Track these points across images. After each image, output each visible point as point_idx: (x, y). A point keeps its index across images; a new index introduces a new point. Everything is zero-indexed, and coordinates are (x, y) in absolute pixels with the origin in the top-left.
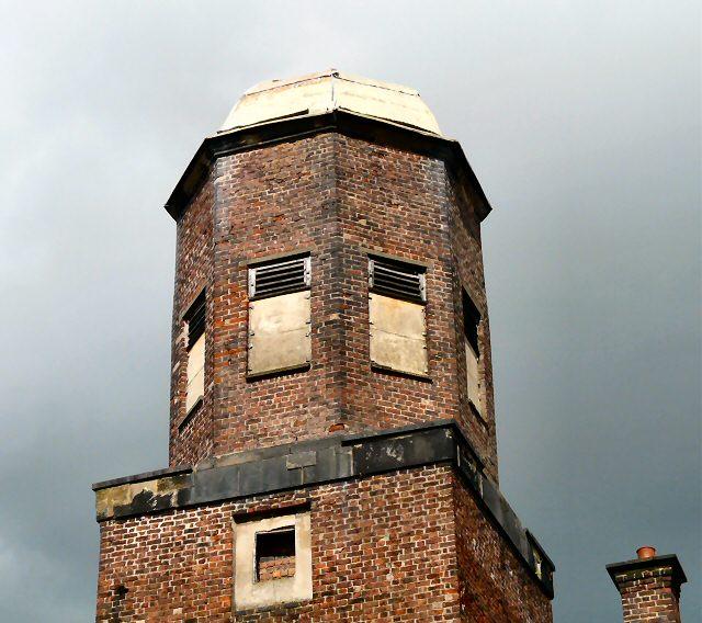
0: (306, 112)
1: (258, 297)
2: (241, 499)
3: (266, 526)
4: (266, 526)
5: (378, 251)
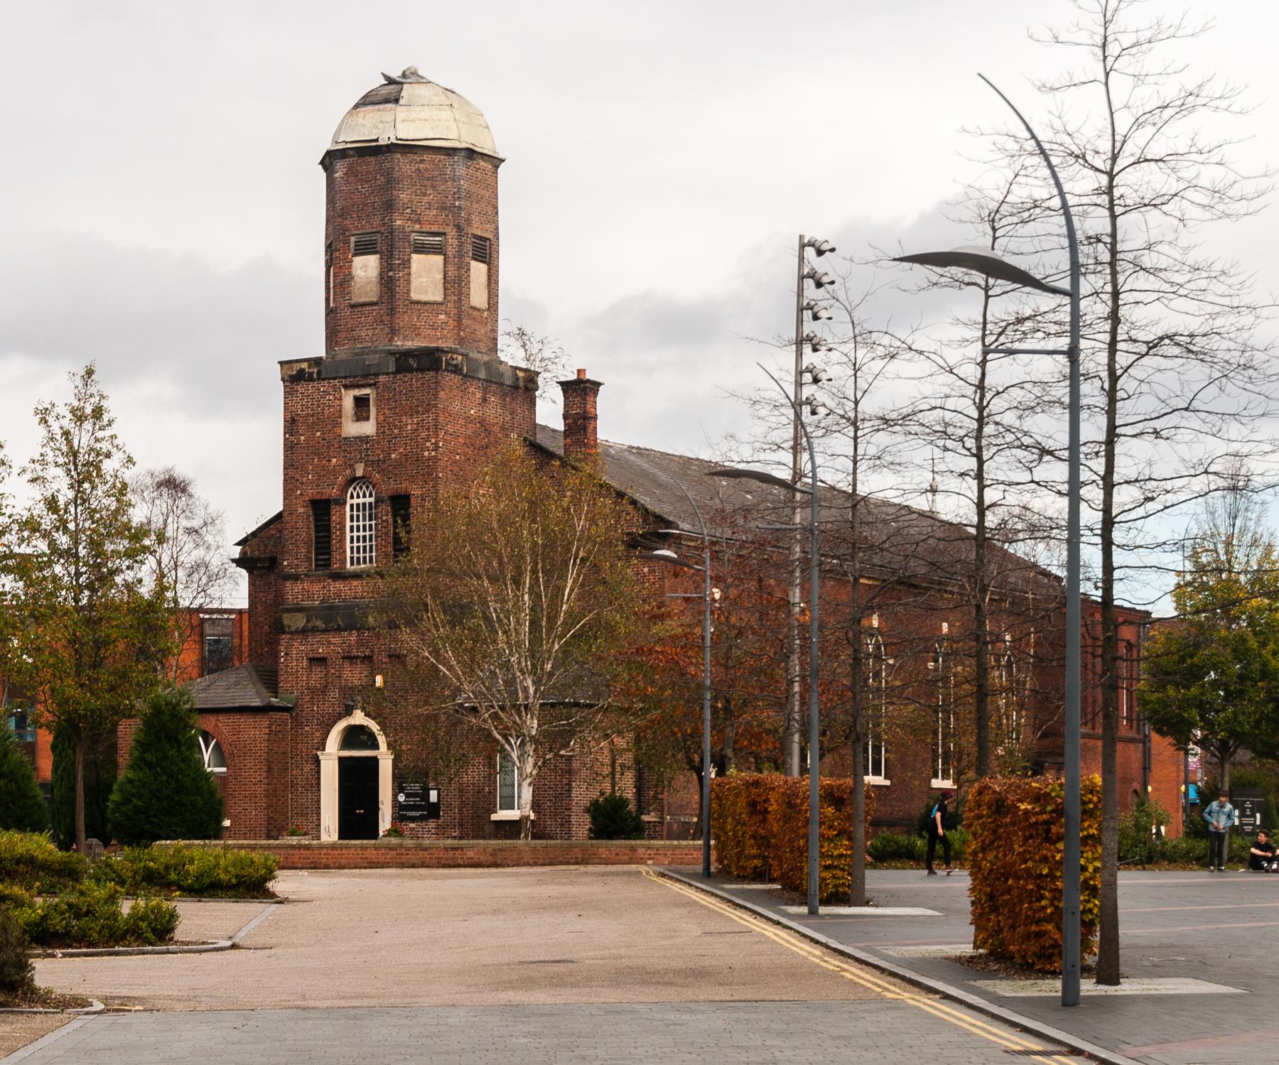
1: (355, 255)
2: (345, 378)
3: (358, 392)
4: (358, 392)
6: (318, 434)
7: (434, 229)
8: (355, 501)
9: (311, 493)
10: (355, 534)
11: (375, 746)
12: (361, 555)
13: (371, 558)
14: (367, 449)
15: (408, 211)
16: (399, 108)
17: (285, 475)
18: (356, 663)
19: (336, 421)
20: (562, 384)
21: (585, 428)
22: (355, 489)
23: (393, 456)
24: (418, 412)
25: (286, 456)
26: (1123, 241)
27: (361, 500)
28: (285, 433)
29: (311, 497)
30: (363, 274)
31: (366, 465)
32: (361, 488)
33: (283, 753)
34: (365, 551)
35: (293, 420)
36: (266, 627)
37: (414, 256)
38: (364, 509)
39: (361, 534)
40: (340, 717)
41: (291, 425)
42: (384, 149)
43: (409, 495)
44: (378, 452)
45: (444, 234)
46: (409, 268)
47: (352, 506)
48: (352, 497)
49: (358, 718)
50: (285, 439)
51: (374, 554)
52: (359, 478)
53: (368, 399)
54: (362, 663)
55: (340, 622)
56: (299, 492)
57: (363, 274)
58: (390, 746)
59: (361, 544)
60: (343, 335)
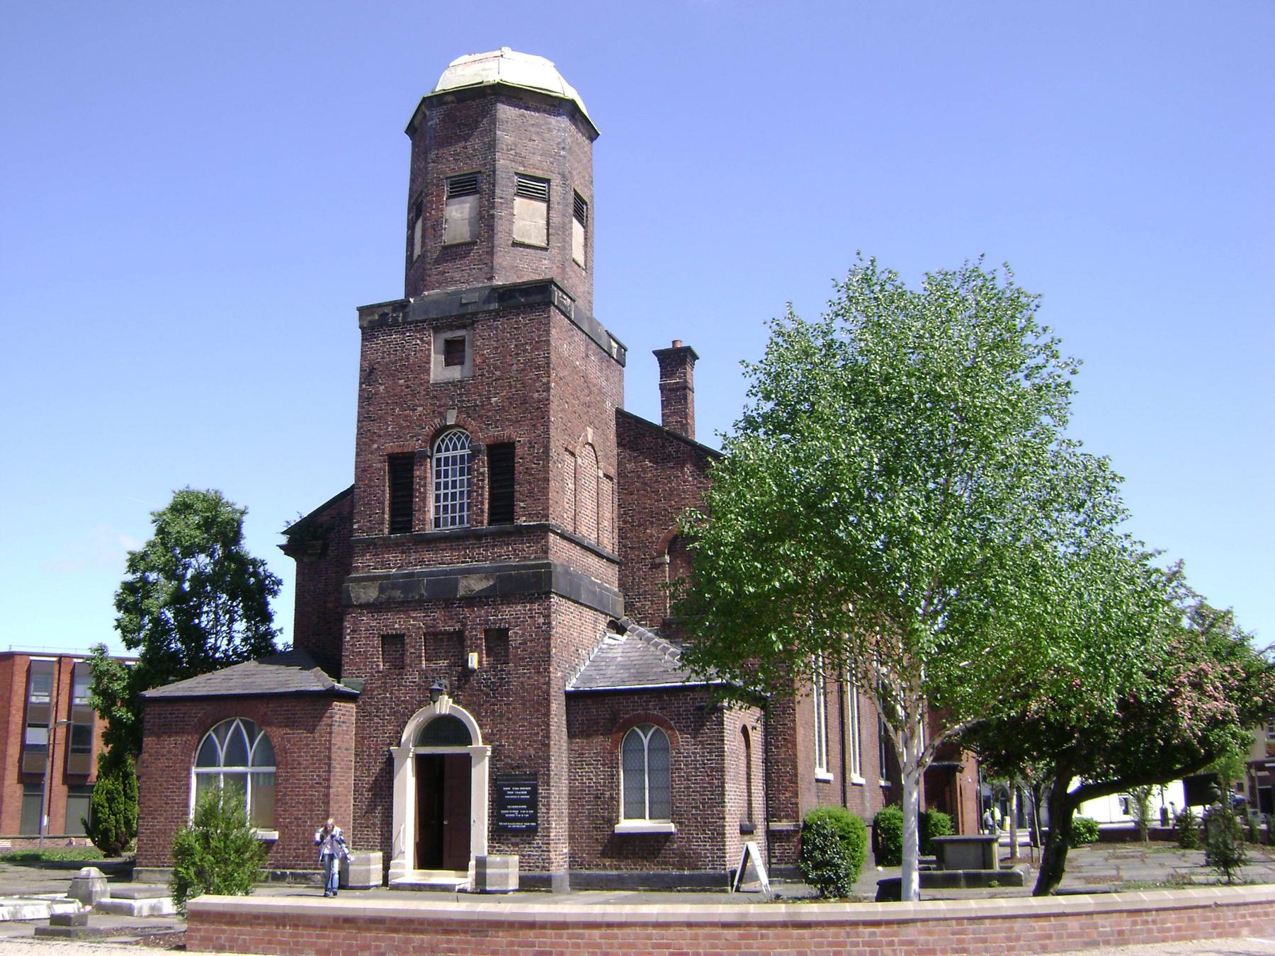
0: (482, 83)
3: (449, 335)
4: (449, 335)
5: (521, 169)
6: (402, 381)
7: (539, 174)
8: (443, 455)
9: (391, 446)
10: (442, 492)
11: (466, 738)
12: (449, 515)
13: (461, 518)
14: (461, 395)
15: (513, 152)
16: (66, 798)
17: (359, 428)
18: (442, 640)
19: (424, 368)
20: (656, 353)
21: (685, 398)
22: (443, 441)
23: (494, 400)
24: (525, 351)
25: (360, 407)
26: (3, 916)
27: (450, 454)
28: (361, 384)
29: (390, 450)
30: (459, 215)
31: (459, 412)
32: (451, 440)
33: (347, 749)
34: (454, 511)
35: (372, 370)
36: (314, 617)
37: (518, 199)
38: (454, 463)
39: (450, 491)
40: (421, 704)
41: (368, 375)
42: (489, 91)
43: (514, 443)
44: (475, 397)
45: (548, 181)
46: (512, 208)
47: (439, 460)
48: (439, 450)
49: (445, 705)
50: (361, 390)
51: (465, 513)
52: (451, 427)
53: (464, 340)
54: (449, 640)
55: (423, 592)
56: (375, 446)
57: (459, 215)
58: (486, 739)
59: (449, 503)
60: (434, 279)
